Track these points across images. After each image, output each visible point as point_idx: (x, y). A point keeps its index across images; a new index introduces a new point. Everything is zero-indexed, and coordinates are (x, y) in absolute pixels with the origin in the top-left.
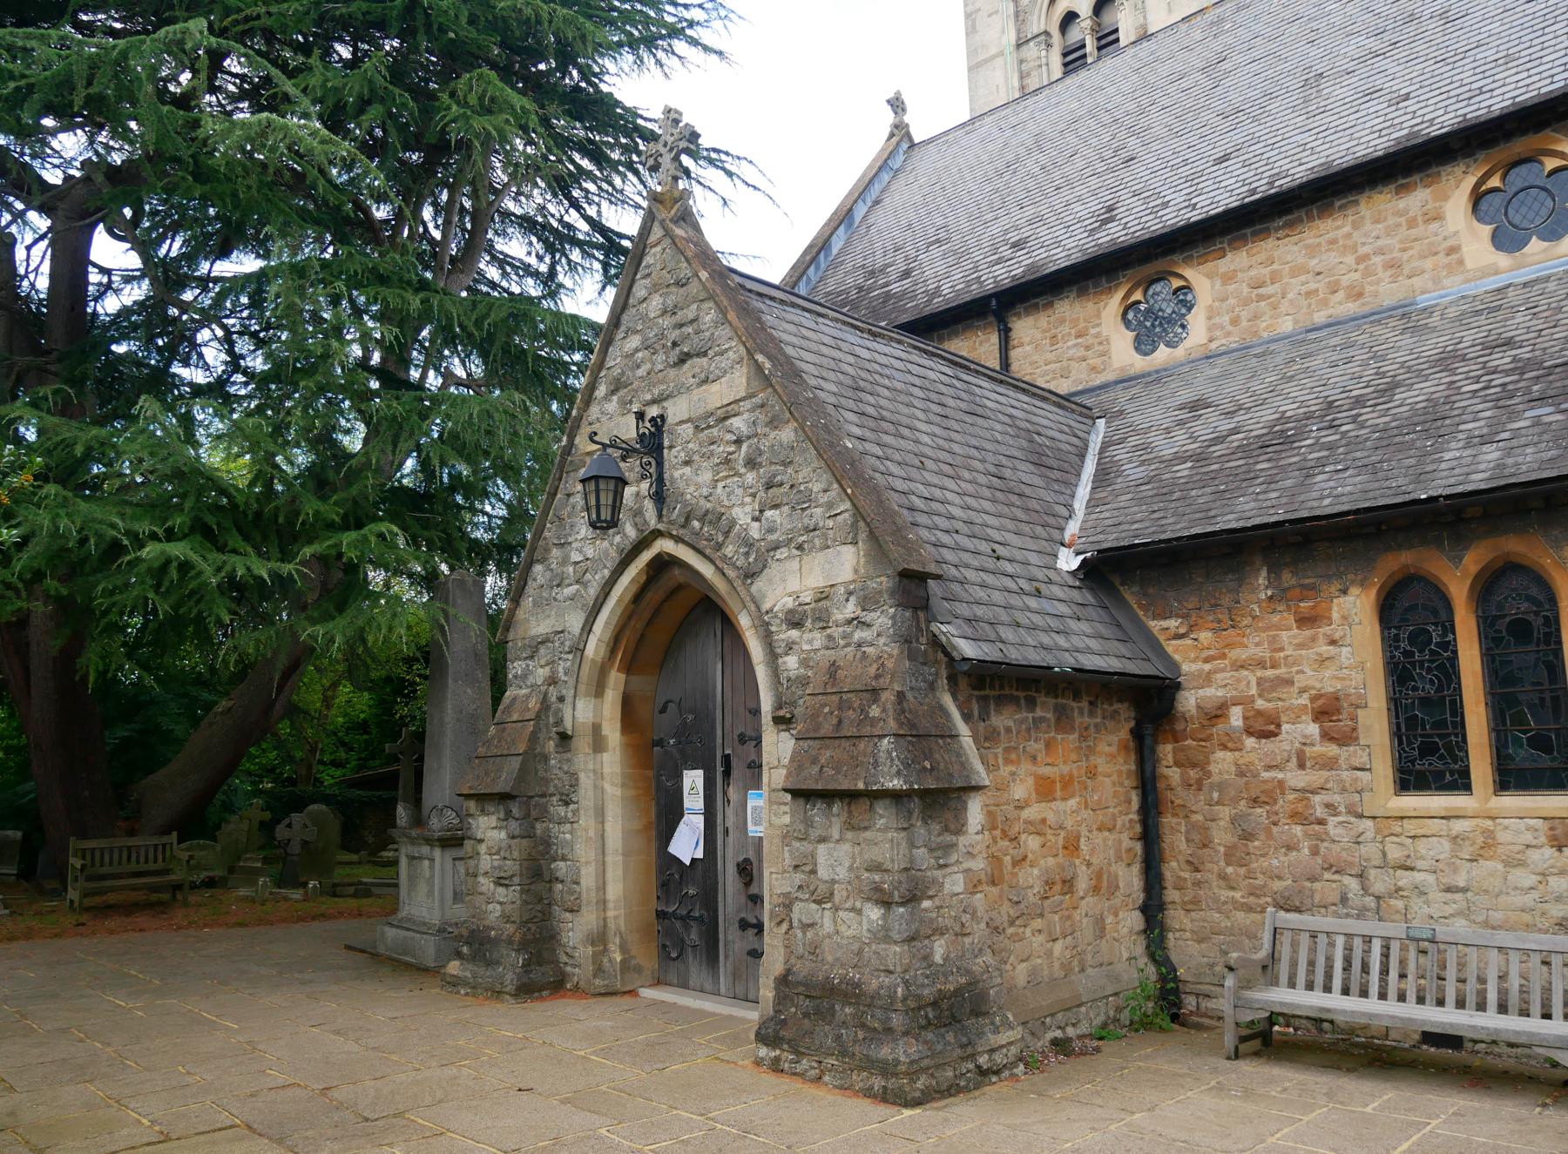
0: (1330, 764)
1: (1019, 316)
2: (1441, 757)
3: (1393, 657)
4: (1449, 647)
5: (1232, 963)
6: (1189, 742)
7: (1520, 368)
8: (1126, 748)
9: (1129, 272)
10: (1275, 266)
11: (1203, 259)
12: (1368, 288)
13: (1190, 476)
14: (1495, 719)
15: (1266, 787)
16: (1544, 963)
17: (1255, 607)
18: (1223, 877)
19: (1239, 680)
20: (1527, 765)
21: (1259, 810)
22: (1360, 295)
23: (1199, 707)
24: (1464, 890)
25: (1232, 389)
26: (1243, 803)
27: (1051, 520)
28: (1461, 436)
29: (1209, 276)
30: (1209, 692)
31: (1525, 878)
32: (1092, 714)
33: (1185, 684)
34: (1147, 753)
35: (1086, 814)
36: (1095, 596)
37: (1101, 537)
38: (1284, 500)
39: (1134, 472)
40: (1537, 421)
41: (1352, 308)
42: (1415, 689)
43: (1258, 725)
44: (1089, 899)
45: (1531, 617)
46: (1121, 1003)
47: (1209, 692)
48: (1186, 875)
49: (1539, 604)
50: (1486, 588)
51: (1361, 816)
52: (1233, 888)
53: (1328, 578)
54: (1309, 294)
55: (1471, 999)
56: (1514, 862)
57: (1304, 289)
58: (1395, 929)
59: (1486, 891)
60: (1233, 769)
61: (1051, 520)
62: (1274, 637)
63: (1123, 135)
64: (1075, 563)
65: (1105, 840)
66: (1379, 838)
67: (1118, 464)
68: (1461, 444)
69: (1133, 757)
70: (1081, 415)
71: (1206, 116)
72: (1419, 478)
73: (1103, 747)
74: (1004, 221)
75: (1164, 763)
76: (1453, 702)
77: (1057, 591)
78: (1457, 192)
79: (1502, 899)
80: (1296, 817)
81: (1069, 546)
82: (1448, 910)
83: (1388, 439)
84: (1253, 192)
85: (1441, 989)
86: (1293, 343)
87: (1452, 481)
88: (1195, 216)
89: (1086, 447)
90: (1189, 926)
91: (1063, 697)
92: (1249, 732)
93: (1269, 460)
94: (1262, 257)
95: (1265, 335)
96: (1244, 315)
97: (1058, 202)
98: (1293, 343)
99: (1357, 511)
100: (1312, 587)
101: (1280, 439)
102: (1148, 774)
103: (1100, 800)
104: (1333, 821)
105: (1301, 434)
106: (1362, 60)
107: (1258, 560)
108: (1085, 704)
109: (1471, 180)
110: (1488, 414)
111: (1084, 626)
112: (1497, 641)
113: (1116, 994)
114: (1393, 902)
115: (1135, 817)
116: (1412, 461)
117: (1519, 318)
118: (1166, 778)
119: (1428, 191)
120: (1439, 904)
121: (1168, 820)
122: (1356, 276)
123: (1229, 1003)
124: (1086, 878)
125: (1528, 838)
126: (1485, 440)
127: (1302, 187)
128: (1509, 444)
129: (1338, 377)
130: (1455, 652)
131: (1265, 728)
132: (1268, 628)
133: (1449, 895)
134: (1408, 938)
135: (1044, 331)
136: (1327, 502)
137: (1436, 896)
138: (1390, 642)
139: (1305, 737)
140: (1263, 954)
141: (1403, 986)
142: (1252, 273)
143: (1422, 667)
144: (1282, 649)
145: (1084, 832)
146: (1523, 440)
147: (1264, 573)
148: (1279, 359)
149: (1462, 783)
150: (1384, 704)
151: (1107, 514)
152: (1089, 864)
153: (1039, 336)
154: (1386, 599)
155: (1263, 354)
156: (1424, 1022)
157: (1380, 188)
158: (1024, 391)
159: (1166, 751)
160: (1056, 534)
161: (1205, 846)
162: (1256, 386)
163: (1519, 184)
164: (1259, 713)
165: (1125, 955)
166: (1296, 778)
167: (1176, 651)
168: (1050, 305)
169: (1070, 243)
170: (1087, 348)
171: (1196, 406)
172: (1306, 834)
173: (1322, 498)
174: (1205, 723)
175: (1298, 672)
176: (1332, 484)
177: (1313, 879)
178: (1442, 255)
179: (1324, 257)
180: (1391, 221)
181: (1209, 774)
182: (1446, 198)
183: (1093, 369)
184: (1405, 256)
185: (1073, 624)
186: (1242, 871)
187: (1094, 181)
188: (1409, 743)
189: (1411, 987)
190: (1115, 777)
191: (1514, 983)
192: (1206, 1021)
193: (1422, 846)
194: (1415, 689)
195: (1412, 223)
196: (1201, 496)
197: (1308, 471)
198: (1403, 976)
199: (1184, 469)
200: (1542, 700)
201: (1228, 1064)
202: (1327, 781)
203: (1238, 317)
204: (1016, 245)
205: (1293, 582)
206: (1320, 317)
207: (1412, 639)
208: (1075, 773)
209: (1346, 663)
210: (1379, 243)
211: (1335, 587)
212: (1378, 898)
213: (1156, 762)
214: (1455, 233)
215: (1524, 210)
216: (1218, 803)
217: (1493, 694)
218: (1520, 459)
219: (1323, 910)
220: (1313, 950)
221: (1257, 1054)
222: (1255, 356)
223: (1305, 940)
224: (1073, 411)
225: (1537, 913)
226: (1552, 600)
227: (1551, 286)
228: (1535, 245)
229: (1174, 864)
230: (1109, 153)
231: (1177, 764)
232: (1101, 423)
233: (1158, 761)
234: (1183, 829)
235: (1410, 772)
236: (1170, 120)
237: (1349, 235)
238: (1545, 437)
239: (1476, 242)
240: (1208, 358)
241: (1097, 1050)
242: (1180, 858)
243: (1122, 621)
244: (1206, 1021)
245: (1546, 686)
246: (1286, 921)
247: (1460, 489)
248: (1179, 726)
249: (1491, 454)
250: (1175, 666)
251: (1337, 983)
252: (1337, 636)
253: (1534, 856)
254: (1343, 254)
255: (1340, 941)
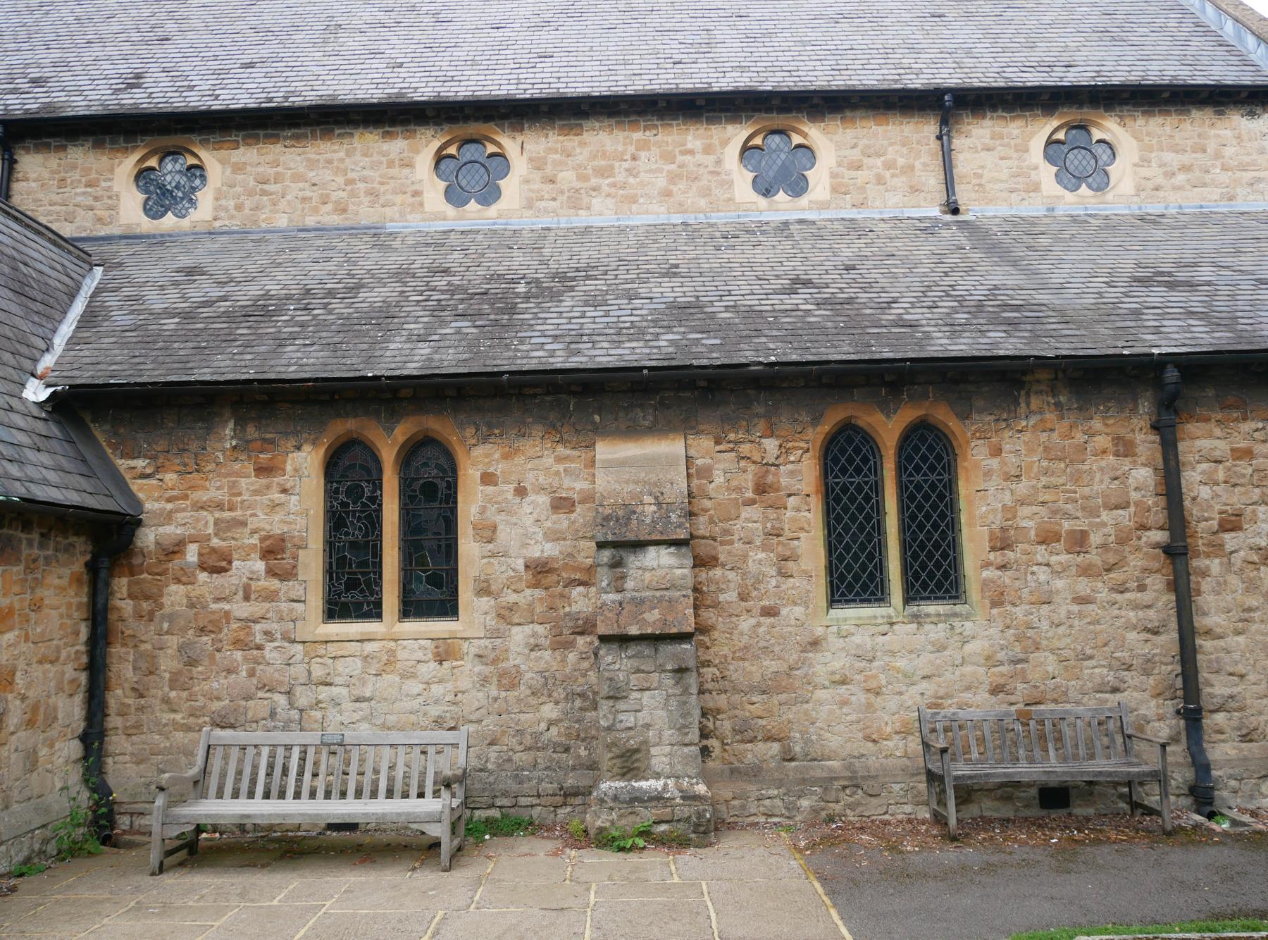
0: (271, 597)
1: (28, 150)
2: (362, 591)
3: (332, 507)
4: (376, 501)
5: (163, 783)
6: (145, 576)
7: (452, 290)
8: (79, 581)
9: (148, 138)
10: (280, 169)
11: (218, 146)
12: (351, 207)
13: (176, 330)
14: (405, 560)
15: (213, 617)
16: (423, 752)
17: (220, 455)
18: (166, 701)
19: (198, 520)
20: (424, 597)
21: (205, 638)
22: (344, 211)
23: (157, 543)
24: (369, 700)
25: (229, 264)
26: (191, 632)
27: (23, 349)
28: (404, 333)
29: (222, 162)
30: (169, 529)
31: (414, 687)
32: (42, 546)
33: (146, 521)
34: (100, 585)
35: (24, 647)
36: (62, 429)
37: (76, 373)
38: (256, 363)
39: (122, 318)
40: (458, 331)
41: (336, 220)
42: (347, 534)
43: (212, 561)
44: (22, 734)
45: (438, 481)
46: (48, 833)
47: (169, 529)
48: (130, 701)
49: (444, 471)
50: (411, 453)
51: (293, 641)
52: (174, 711)
53: (286, 435)
54: (304, 199)
55: (367, 790)
56: (408, 675)
57: (301, 194)
58: (312, 738)
59: (386, 699)
60: (185, 601)
61: (23, 349)
62: (234, 483)
63: (162, 15)
64: (44, 395)
65: (44, 673)
66: (306, 660)
67: (108, 309)
68: (403, 339)
69: (86, 589)
70: (78, 257)
71: (239, 26)
72: (368, 360)
73: (53, 580)
74: (28, 55)
75: (119, 595)
76: (375, 546)
77: (18, 420)
78: (426, 150)
79: (397, 704)
80: (239, 644)
81: (41, 378)
82: (356, 716)
83: (348, 326)
84: (270, 100)
85: (345, 783)
86: (286, 237)
87: (393, 366)
88: (217, 105)
89: (78, 288)
90: (129, 749)
91: (10, 527)
92: (203, 567)
93: (249, 328)
94: (270, 158)
95: (263, 225)
96: (248, 204)
97: (87, 54)
98: (286, 237)
99: (316, 380)
100: (272, 442)
101: (261, 311)
102: (99, 606)
103: (43, 633)
104: (269, 646)
105: (280, 311)
106: (373, 26)
107: (227, 412)
108: (35, 536)
109: (436, 144)
110: (426, 319)
111: (44, 458)
112: (412, 498)
113: (44, 826)
114: (313, 713)
115: (83, 648)
116: (365, 346)
117: (456, 255)
118: (119, 609)
119: (406, 142)
120: (350, 711)
121: (116, 650)
122: (342, 194)
123: (161, 821)
124: (19, 712)
125: (419, 655)
126: (421, 339)
127: (310, 108)
128: (437, 344)
129: (318, 271)
130: (380, 505)
131: (217, 564)
132: (229, 475)
133: (358, 704)
134: (323, 744)
135: (53, 172)
136: (292, 368)
137: (348, 706)
138: (331, 494)
139: (252, 572)
140: (194, 771)
141: (315, 784)
142: (260, 169)
143: (354, 516)
144: (240, 494)
145: (21, 665)
146: (447, 343)
147: (231, 425)
148: (271, 248)
149: (374, 612)
150: (321, 546)
151: (87, 353)
152: (24, 698)
153: (47, 176)
154: (332, 457)
155: (259, 241)
156: (328, 815)
157: (371, 129)
158: (16, 219)
159: (121, 584)
160: (27, 364)
161: (151, 673)
162: (248, 265)
163: (468, 157)
164: (214, 550)
165: (59, 785)
166: (241, 609)
167: (140, 489)
168: (64, 148)
169: (93, 95)
170: (96, 199)
171: (192, 272)
172: (246, 659)
173: (289, 365)
174: (162, 558)
175: (252, 515)
176: (299, 355)
177: (248, 698)
178: (408, 195)
179: (321, 172)
180: (375, 158)
181: (161, 606)
182: (418, 152)
183: (100, 220)
184: (383, 188)
185: (31, 455)
186: (185, 694)
187: (127, 47)
188: (338, 579)
189: (320, 784)
190: (63, 610)
191: (399, 773)
192: (138, 838)
193: (340, 664)
194: (347, 534)
195: (391, 164)
196: (183, 349)
197: (280, 342)
198: (315, 775)
199: (171, 324)
200: (439, 546)
201: (151, 880)
202: (268, 611)
203: (243, 204)
204: (36, 82)
205: (256, 435)
206: (310, 221)
207: (349, 492)
208: (17, 606)
209: (293, 509)
210: (365, 173)
211: (292, 442)
212: (301, 711)
213: (109, 594)
214: (421, 181)
215: (469, 177)
216: (167, 633)
217: (405, 541)
218: (444, 357)
219: (254, 725)
220: (241, 761)
221: (181, 864)
222: (252, 241)
223: (235, 753)
224: (70, 252)
225: (421, 714)
226: (454, 470)
227: (480, 238)
228: (473, 205)
229: (119, 692)
230: (145, 27)
231: (131, 596)
232: (98, 271)
233: (112, 593)
234: (131, 658)
235: (336, 604)
236: (209, 18)
237: (342, 160)
238: (463, 343)
239: (434, 191)
240: (210, 233)
241: (13, 889)
242: (127, 685)
243: (89, 457)
244: (138, 838)
245: (443, 536)
246: (220, 738)
247: (398, 373)
248: (137, 561)
249: (424, 350)
250: (138, 504)
251: (260, 789)
252: (288, 486)
253: (423, 669)
254: (336, 174)
255: (265, 752)
